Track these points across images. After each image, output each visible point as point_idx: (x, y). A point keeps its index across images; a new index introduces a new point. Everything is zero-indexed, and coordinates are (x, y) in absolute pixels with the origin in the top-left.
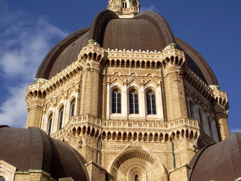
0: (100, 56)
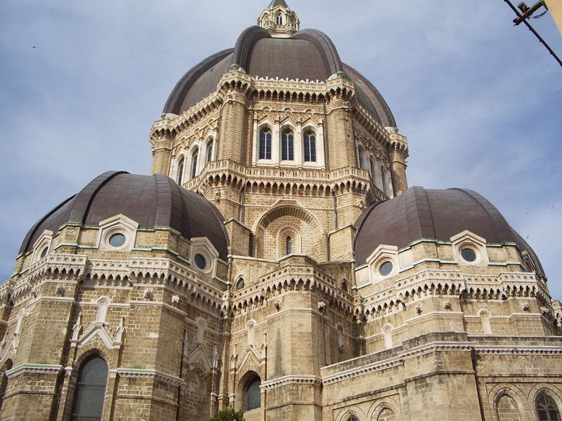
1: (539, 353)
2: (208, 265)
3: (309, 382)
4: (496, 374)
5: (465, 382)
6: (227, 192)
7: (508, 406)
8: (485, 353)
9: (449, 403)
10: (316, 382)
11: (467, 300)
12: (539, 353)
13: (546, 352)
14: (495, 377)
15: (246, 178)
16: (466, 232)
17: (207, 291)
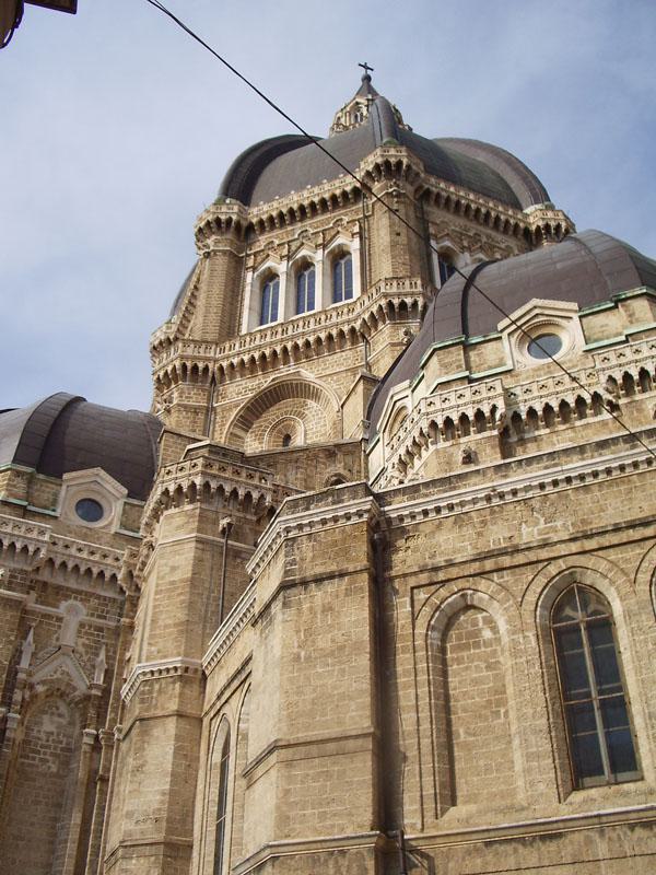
0: (558, 226)
1: (563, 486)
2: (106, 514)
3: (172, 673)
4: (440, 560)
5: (342, 596)
6: (181, 393)
7: (476, 634)
8: (420, 518)
9: (295, 650)
10: (186, 670)
11: (527, 436)
12: (563, 486)
13: (582, 477)
14: (436, 569)
15: (216, 361)
16: (535, 302)
17: (85, 555)
